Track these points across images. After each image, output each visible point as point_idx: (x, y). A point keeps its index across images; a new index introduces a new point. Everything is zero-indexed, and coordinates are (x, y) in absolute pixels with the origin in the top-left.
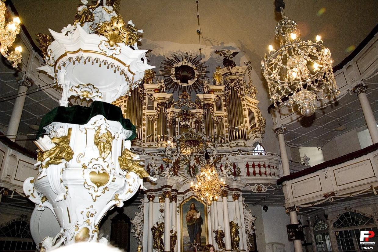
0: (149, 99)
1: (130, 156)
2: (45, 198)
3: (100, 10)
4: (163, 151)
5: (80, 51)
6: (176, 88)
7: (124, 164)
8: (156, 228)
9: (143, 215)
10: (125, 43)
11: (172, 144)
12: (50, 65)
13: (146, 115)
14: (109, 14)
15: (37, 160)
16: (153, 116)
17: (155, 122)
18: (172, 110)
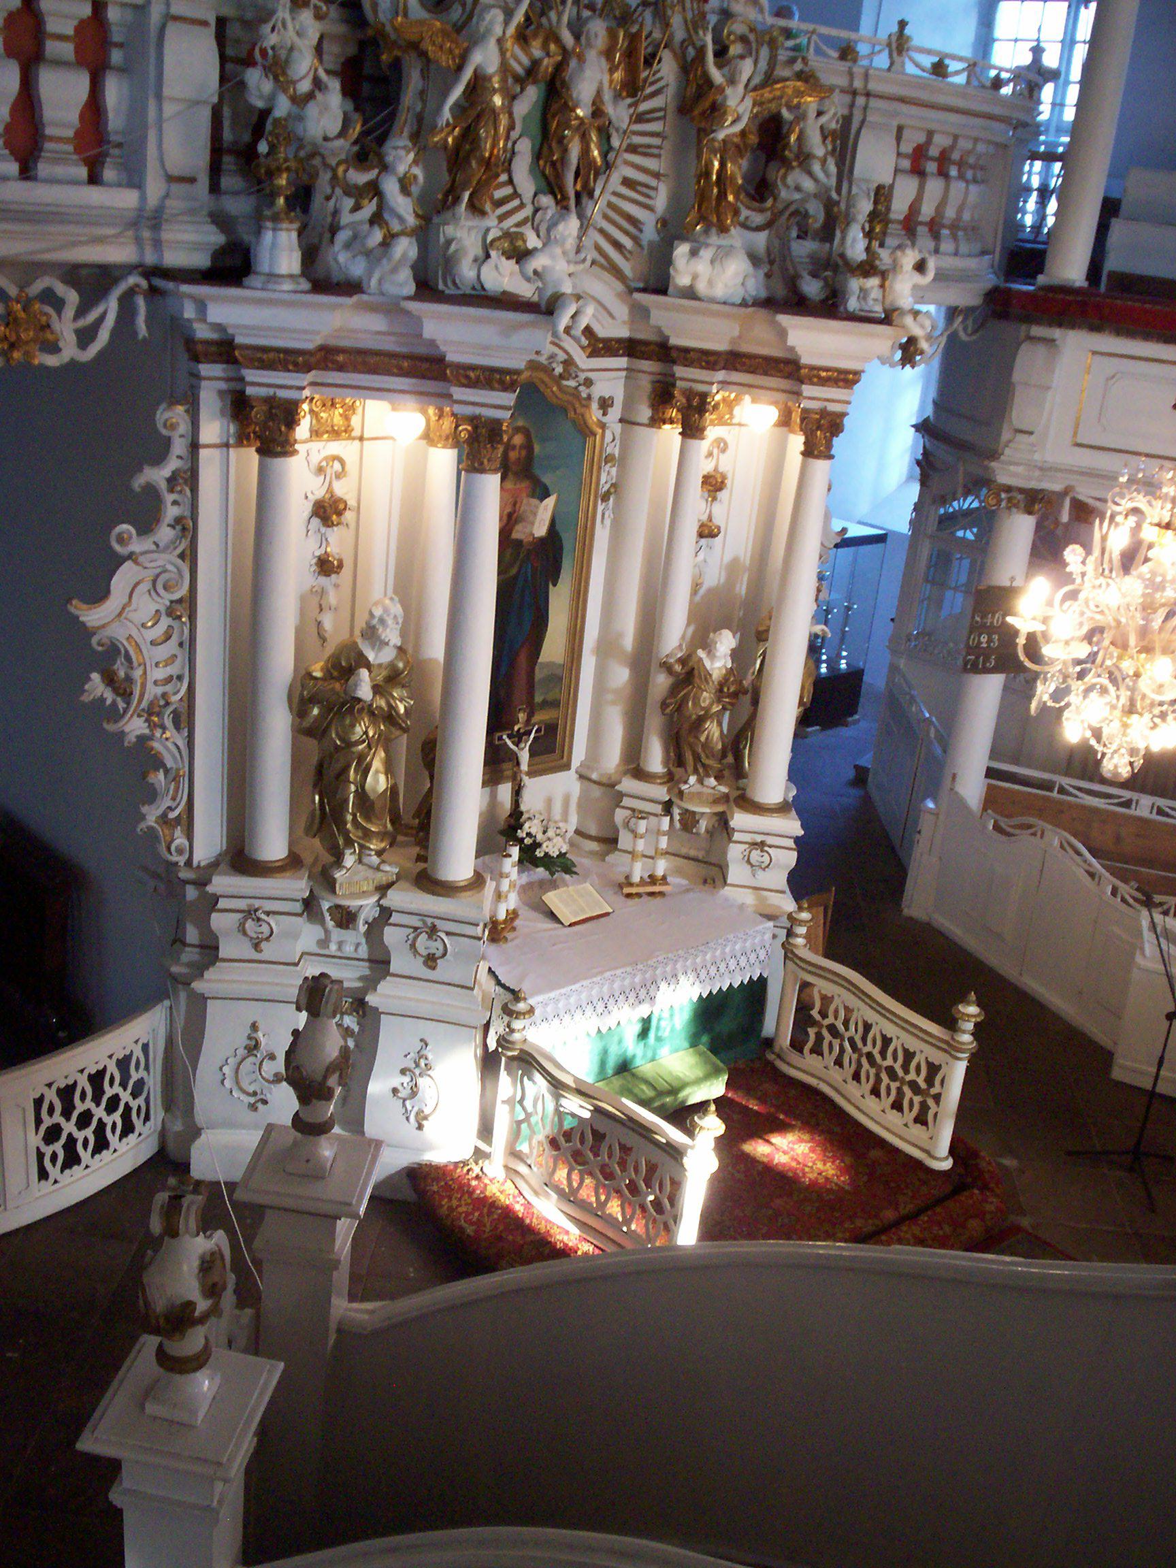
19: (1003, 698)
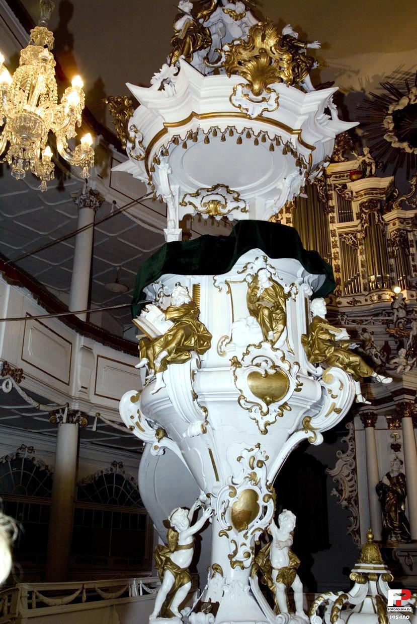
0: (339, 196)
1: (327, 332)
2: (162, 433)
3: (218, 17)
4: (384, 312)
5: (194, 119)
6: (401, 164)
7: (317, 352)
8: (386, 486)
9: (355, 458)
10: (286, 82)
11: (405, 294)
12: (137, 158)
13: (337, 234)
14: (238, 22)
15: (139, 357)
16: (354, 233)
17: (360, 247)
18: (395, 216)
19: (139, 465)
